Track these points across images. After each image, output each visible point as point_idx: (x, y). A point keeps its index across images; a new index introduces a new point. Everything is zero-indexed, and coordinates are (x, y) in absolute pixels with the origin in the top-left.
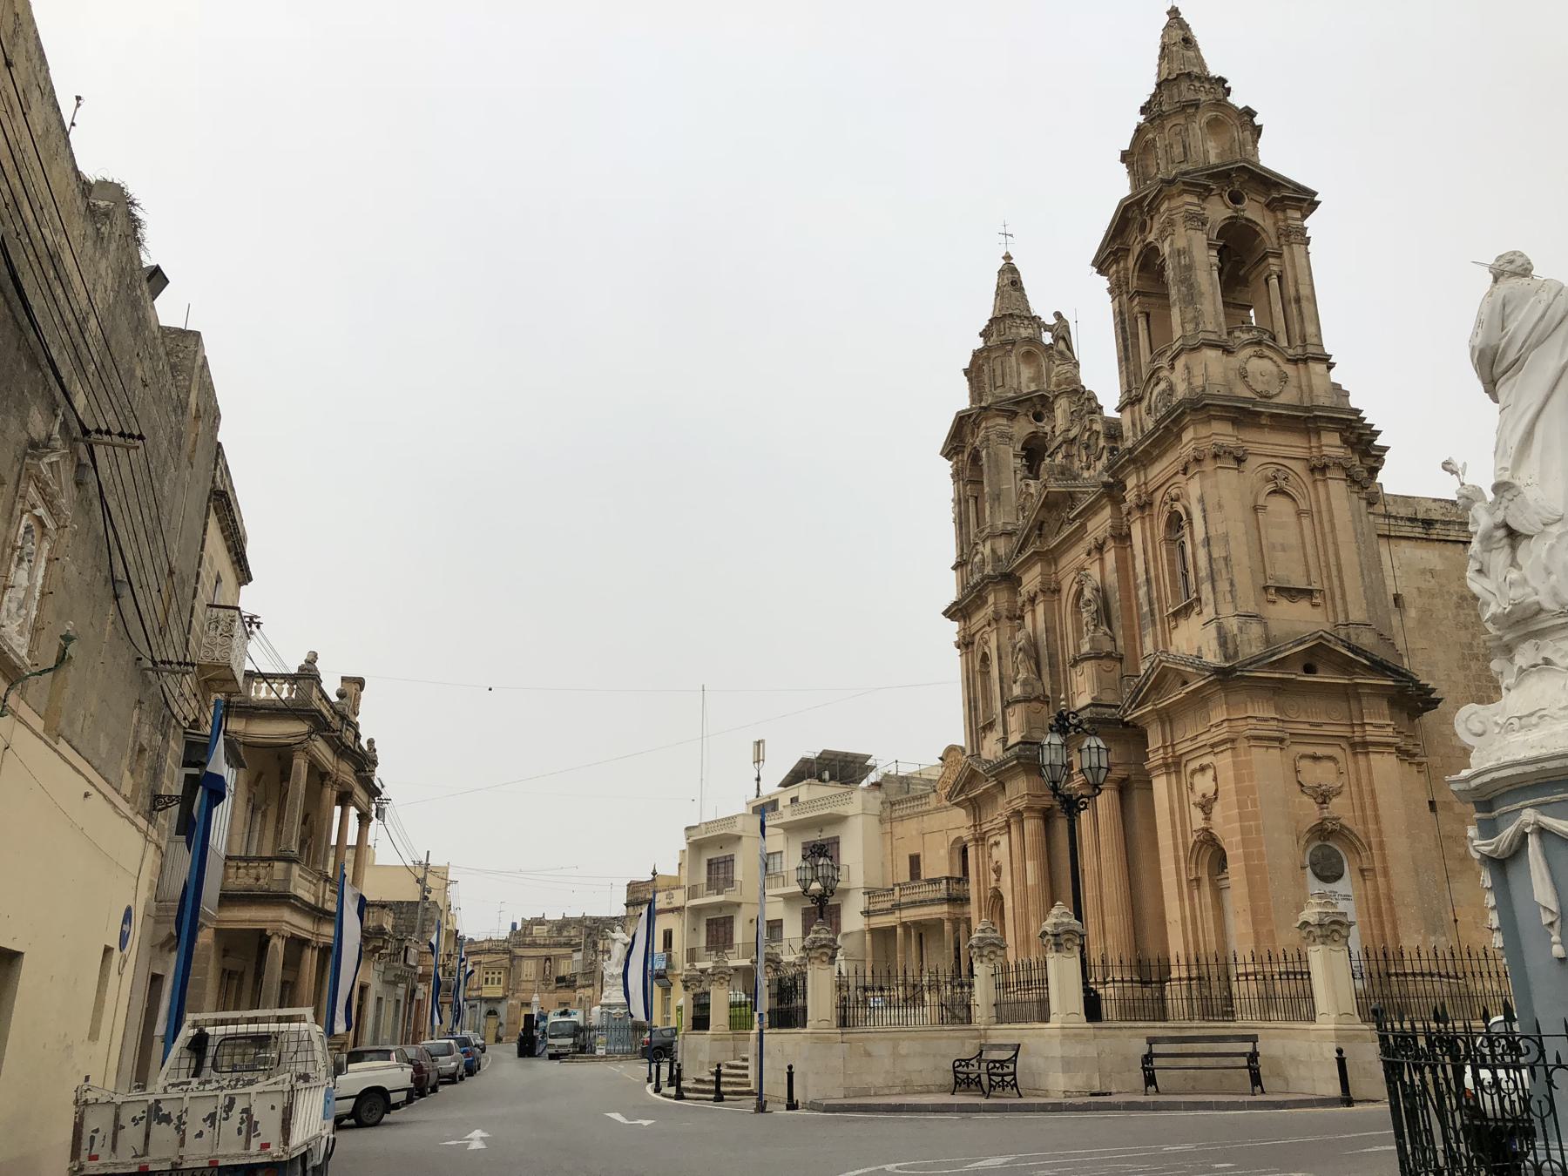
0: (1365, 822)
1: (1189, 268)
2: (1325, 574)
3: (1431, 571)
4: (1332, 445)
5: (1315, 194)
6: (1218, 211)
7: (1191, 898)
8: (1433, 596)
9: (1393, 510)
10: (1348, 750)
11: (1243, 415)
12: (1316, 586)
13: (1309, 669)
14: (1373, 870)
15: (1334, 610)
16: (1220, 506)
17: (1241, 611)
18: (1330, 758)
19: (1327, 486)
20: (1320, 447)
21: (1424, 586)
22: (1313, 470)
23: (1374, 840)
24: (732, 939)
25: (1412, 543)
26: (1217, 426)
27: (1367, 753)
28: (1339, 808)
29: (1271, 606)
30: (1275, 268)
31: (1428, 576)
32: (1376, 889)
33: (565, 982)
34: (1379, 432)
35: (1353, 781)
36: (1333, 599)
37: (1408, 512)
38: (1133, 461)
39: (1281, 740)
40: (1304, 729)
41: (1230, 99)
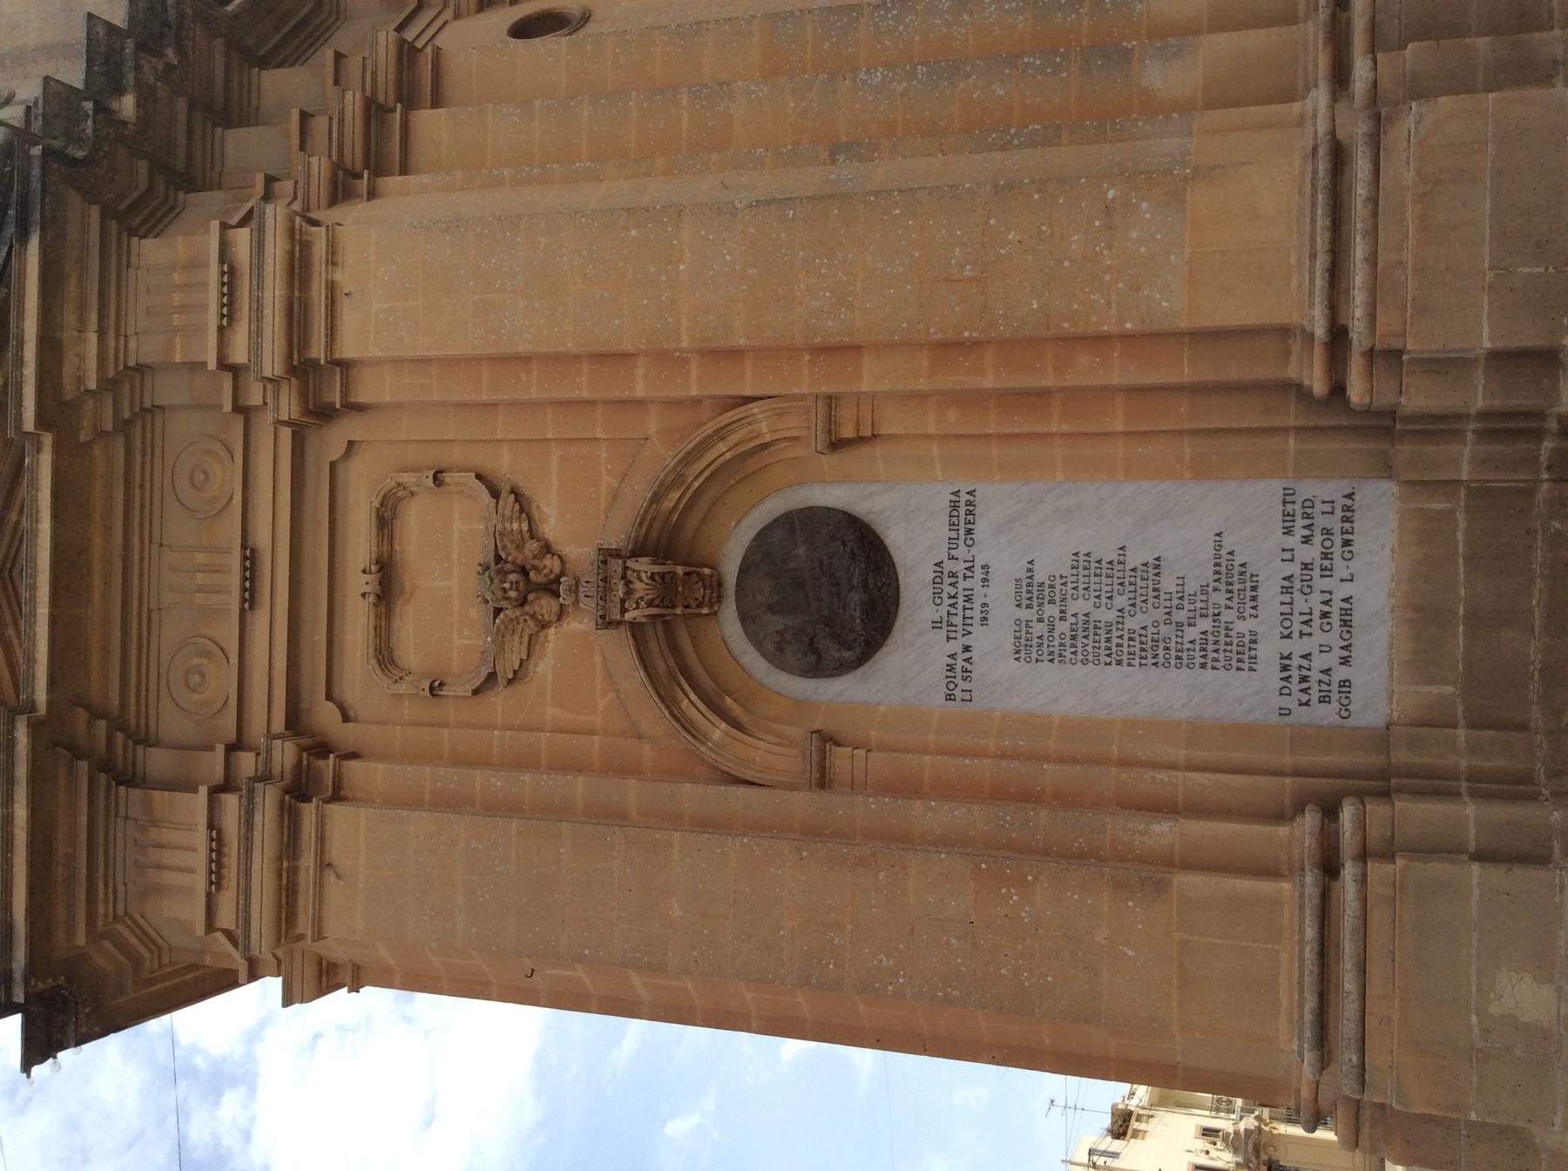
14: (831, 401)
18: (385, 522)
27: (345, 366)
28: (580, 517)
33: (1179, 625)
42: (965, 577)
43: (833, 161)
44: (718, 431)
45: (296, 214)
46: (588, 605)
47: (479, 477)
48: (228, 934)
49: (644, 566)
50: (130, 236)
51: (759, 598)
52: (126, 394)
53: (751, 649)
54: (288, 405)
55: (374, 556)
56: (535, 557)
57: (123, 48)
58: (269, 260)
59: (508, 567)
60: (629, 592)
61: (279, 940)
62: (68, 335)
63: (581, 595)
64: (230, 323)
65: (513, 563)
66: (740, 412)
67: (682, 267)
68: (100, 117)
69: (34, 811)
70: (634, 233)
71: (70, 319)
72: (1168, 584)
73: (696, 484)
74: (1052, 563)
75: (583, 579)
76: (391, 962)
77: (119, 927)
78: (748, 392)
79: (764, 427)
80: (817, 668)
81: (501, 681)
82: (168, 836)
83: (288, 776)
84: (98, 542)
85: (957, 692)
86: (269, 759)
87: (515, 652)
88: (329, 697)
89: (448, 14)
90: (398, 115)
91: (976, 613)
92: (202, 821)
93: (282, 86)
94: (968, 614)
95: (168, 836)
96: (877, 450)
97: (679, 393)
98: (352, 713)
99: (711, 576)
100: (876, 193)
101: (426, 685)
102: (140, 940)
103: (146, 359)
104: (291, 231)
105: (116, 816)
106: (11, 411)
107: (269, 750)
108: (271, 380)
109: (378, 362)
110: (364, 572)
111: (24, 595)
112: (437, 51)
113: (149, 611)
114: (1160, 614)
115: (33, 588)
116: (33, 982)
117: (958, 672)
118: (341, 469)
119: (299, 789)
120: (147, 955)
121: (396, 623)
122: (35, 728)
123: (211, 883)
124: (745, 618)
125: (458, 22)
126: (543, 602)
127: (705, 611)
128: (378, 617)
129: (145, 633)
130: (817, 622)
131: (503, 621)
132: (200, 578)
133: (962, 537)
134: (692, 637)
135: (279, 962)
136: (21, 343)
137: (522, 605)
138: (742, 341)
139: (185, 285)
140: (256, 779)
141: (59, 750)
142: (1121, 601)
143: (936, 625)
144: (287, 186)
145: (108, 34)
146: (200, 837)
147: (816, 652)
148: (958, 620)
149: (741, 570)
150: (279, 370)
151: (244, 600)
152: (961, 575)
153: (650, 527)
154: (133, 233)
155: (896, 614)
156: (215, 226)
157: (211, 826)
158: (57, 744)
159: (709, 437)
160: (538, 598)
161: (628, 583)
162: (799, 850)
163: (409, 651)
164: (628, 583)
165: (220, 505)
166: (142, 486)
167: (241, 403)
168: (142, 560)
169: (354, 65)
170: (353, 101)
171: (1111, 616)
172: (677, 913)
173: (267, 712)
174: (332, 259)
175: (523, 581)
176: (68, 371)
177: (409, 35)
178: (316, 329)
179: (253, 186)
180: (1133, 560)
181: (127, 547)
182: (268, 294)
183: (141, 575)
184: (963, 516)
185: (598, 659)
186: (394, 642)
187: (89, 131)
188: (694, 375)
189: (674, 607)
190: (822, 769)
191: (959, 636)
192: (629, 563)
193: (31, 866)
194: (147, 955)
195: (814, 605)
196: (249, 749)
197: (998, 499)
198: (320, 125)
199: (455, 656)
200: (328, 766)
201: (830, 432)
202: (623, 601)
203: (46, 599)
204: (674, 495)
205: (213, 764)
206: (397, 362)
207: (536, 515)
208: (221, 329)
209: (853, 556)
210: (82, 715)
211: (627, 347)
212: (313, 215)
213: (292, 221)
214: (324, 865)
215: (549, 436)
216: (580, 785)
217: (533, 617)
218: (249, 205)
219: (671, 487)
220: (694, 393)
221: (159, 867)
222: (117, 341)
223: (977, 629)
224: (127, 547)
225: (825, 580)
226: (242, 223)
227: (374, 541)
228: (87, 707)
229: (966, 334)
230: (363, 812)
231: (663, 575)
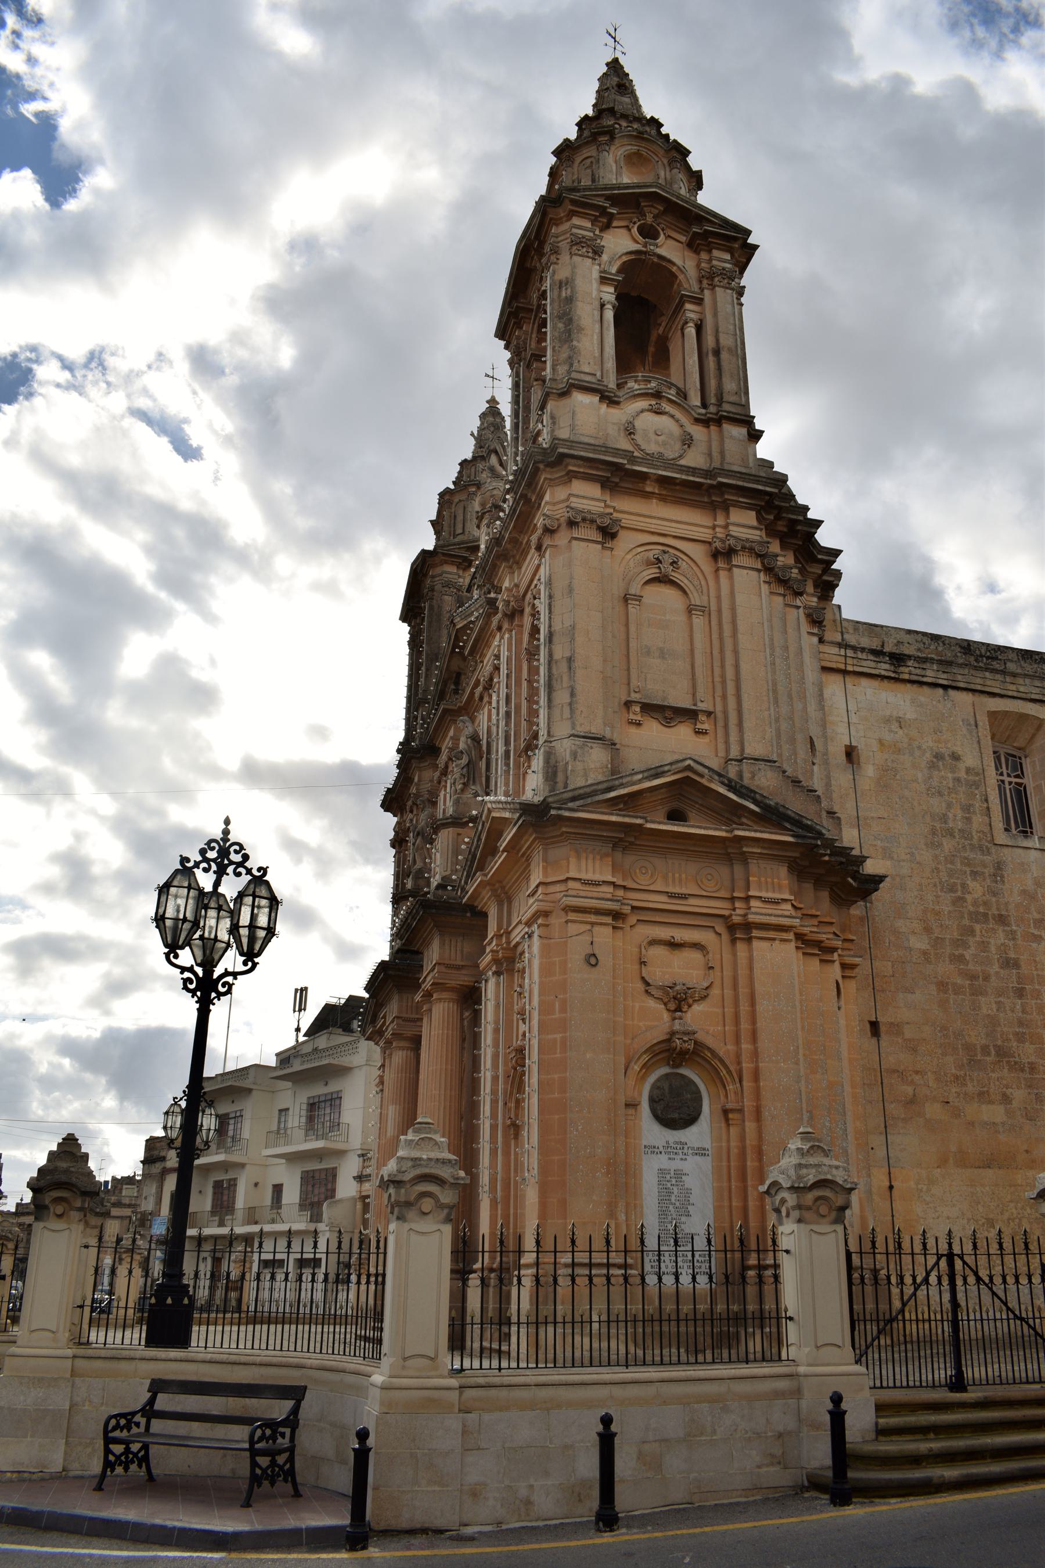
0: (737, 1041)
1: (570, 300)
2: (719, 692)
3: (899, 721)
4: (743, 524)
6: (620, 243)
7: (507, 1153)
8: (899, 751)
9: (851, 639)
10: (725, 937)
11: (618, 475)
12: (702, 706)
13: (675, 816)
14: (741, 1111)
15: (727, 742)
16: (570, 590)
17: (580, 730)
18: (696, 946)
19: (731, 578)
20: (726, 527)
21: (888, 737)
22: (715, 555)
23: (746, 1065)
24: (234, 1203)
25: (875, 683)
26: (579, 487)
27: (749, 940)
28: (700, 1018)
29: (633, 730)
30: (692, 315)
31: (895, 726)
32: (742, 1138)
34: (818, 523)
35: (728, 982)
36: (726, 727)
37: (875, 644)
38: (503, 556)
39: (617, 915)
40: (659, 901)
41: (704, 198)
66: (737, 1080)
72: (683, 1219)
74: (689, 1181)
80: (652, 1101)
91: (672, 1156)
96: (723, 1125)
104: (792, 927)
114: (674, 1216)
117: (653, 1149)
124: (667, 1075)
132: (677, 875)
142: (678, 1204)
143: (667, 1142)
150: (750, 920)
157: (603, 882)
171: (673, 1201)
174: (782, 940)
175: (678, 1000)
180: (690, 1208)
184: (701, 1152)
185: (656, 1023)
197: (706, 1164)
223: (667, 1156)
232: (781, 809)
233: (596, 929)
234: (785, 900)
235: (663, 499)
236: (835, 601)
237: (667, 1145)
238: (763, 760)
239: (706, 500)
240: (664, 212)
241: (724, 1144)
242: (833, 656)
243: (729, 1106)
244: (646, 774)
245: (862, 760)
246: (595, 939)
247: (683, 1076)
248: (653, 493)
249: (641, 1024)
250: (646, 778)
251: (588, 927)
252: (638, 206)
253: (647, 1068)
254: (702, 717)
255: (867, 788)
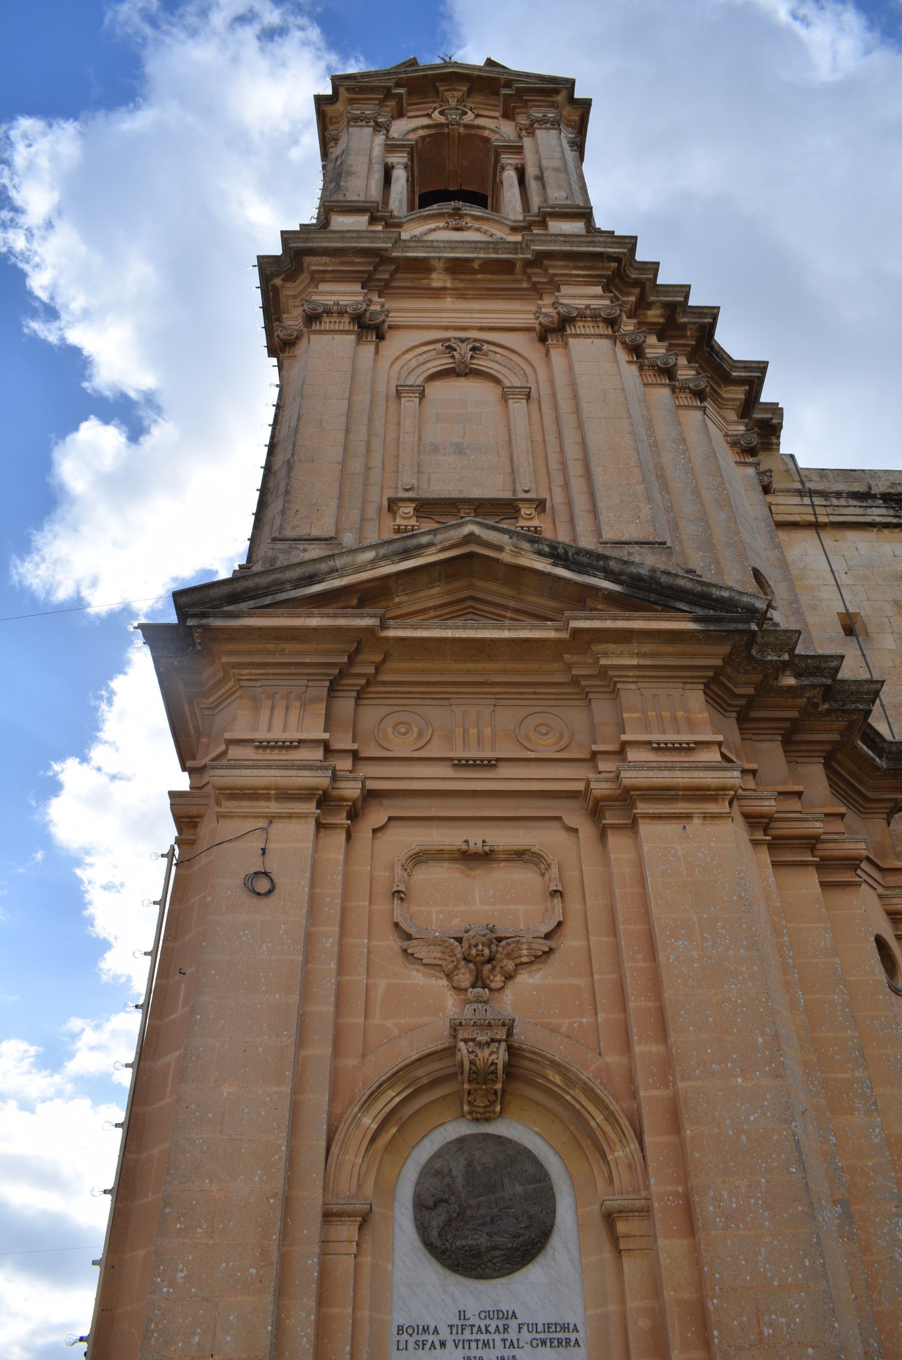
5: (778, 404)
14: (646, 1212)
18: (521, 856)
23: (650, 1094)
25: (871, 535)
27: (632, 826)
28: (524, 996)
42: (504, 1340)
43: (835, 1202)
44: (612, 1114)
45: (736, 791)
46: (468, 1013)
47: (560, 924)
48: (224, 753)
49: (501, 1057)
50: (704, 683)
51: (477, 1153)
52: (598, 683)
53: (436, 1147)
54: (600, 788)
55: (495, 848)
56: (502, 968)
57: (826, 677)
58: (701, 774)
59: (494, 948)
60: (480, 1045)
61: (219, 789)
62: (635, 647)
63: (475, 1006)
64: (654, 749)
65: (497, 952)
66: (630, 1133)
67: (740, 1080)
68: (779, 664)
69: (315, 629)
70: (760, 1040)
71: (646, 648)
73: (568, 1097)
75: (488, 1007)
76: (196, 867)
77: (231, 683)
78: (647, 1139)
79: (619, 1153)
80: (421, 1206)
81: (405, 944)
82: (294, 714)
83: (336, 793)
84: (497, 666)
85: (405, 1336)
86: (348, 779)
87: (421, 952)
88: (390, 819)
89: (880, 890)
90: (811, 859)
92: (304, 736)
93: (814, 779)
94: (473, 1345)
95: (294, 714)
96: (608, 1255)
97: (640, 1079)
98: (379, 835)
99: (494, 1112)
100: (819, 1243)
101: (402, 888)
102: (221, 696)
103: (622, 694)
105: (309, 680)
106: (583, 613)
107: (355, 779)
108: (618, 776)
109: (638, 849)
110: (484, 842)
111: (449, 622)
112: (857, 885)
113: (449, 699)
115: (465, 628)
116: (199, 630)
118: (556, 824)
119: (325, 800)
120: (211, 700)
121: (446, 865)
122: (370, 630)
123: (261, 742)
124: (461, 1141)
125: (876, 898)
126: (468, 976)
127: (466, 1108)
128: (451, 852)
129: (433, 696)
130: (460, 1205)
131: (452, 945)
132: (473, 731)
133: (539, 1336)
134: (444, 1097)
135: (200, 788)
136: (627, 619)
137: (465, 959)
138: (688, 1132)
139: (676, 720)
140: (334, 771)
141: (355, 645)
143: (462, 1315)
144: (751, 784)
145: (834, 668)
146: (293, 735)
147: (436, 1205)
148: (467, 1335)
149: (499, 1137)
150: (626, 782)
151: (459, 760)
152: (506, 1336)
153: (531, 1060)
154: (706, 685)
155: (470, 1277)
156: (720, 738)
157: (300, 741)
158: (359, 643)
159: (607, 1108)
160: (470, 971)
161: (488, 1044)
162: (274, 1196)
163: (426, 875)
164: (488, 1044)
165: (526, 744)
166: (535, 693)
167: (599, 756)
168: (485, 693)
169: (837, 826)
170: (817, 827)
172: (226, 1091)
173: (380, 776)
174: (706, 817)
175: (484, 960)
176: (611, 647)
177: (864, 865)
178: (663, 806)
179: (748, 762)
181: (493, 684)
182: (678, 774)
183: (474, 693)
186: (432, 864)
187: (769, 658)
188: (656, 1093)
189: (469, 1081)
190: (340, 1214)
191: (454, 1337)
192: (503, 1045)
193: (278, 629)
194: (211, 700)
195: (474, 1202)
196: (354, 765)
198: (794, 805)
199: (423, 908)
200: (341, 819)
201: (620, 1211)
202: (473, 1040)
203: (457, 636)
204: (558, 1079)
205: (343, 742)
206: (640, 863)
207: (535, 967)
208: (650, 743)
209: (517, 1236)
210: (378, 658)
211: (672, 1038)
212: (735, 803)
213: (731, 789)
214: (272, 819)
215: (596, 977)
216: (324, 1008)
217: (456, 967)
218: (735, 760)
219: (564, 1077)
220: (642, 1094)
221: (272, 708)
222: (633, 677)
224: (493, 684)
225: (495, 1210)
226: (723, 755)
227: (507, 848)
228: (384, 661)
229: (716, 1333)
230: (310, 845)
231: (494, 1072)
232: (664, 579)
233: (279, 827)
234: (707, 744)
235: (461, 294)
236: (784, 449)
237: (462, 1323)
238: (636, 543)
239: (525, 285)
240: (469, 93)
241: (613, 1308)
242: (791, 507)
243: (615, 1203)
244: (382, 551)
245: (870, 629)
246: (271, 846)
247: (500, 1140)
248: (444, 289)
249: (389, 1023)
250: (385, 557)
251: (262, 823)
252: (437, 92)
253: (398, 1125)
254: (525, 510)
255: (891, 664)
